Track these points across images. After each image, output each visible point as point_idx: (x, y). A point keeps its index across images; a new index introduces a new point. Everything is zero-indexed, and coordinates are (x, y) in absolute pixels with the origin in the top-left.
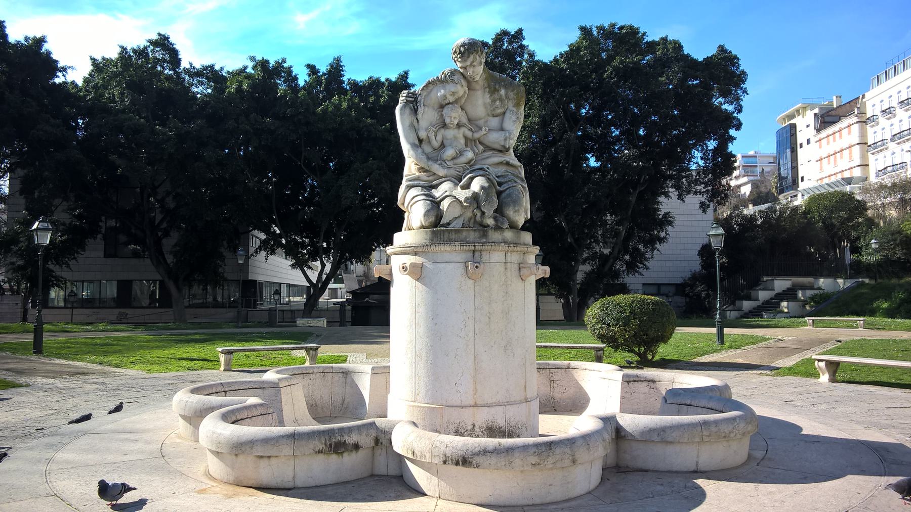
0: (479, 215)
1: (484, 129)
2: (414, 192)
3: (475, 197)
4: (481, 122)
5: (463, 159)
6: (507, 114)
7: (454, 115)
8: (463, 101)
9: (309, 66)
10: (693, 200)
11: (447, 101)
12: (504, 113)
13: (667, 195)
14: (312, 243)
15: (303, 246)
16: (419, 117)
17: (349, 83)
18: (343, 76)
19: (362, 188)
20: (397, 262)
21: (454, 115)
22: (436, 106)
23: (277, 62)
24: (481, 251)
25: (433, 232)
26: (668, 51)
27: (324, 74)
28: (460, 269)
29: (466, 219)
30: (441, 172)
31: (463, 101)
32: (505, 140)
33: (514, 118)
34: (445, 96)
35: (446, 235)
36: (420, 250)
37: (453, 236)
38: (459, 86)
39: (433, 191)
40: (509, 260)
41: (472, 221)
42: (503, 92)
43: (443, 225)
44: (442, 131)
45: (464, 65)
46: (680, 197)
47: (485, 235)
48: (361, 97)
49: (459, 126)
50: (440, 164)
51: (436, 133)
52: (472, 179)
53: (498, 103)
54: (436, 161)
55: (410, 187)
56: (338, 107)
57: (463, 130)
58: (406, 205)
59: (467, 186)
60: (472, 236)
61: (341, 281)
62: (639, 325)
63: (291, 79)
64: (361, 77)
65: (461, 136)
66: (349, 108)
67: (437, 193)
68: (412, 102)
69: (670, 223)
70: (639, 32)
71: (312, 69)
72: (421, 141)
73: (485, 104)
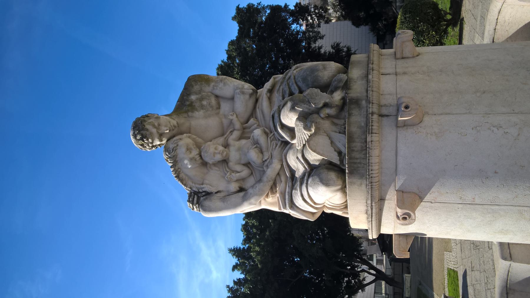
0: (327, 111)
1: (231, 117)
2: (299, 202)
3: (304, 118)
4: (225, 122)
5: (262, 140)
6: (217, 92)
7: (214, 151)
8: (200, 140)
9: (233, 270)
10: (324, 29)
11: (198, 157)
12: (217, 97)
13: (320, 48)
14: (347, 276)
15: (349, 282)
16: (214, 190)
17: (244, 244)
18: (240, 248)
19: (312, 240)
20: (391, 226)
21: (214, 151)
22: (205, 170)
23: (229, 291)
24: (380, 106)
25: (351, 173)
26: (233, 49)
27: (239, 260)
28: (405, 135)
29: (334, 128)
30: (276, 166)
31: (200, 140)
32: (243, 93)
33: (221, 85)
34: (191, 160)
35: (356, 155)
36: (376, 194)
37: (357, 145)
38: (181, 143)
39: (298, 174)
40: (391, 70)
41: (336, 121)
42: (193, 97)
43: (342, 161)
44: (231, 164)
45: (156, 135)
46: (322, 38)
47: (356, 102)
48: (253, 238)
49: (226, 146)
50: (267, 166)
51: (233, 171)
52: (283, 126)
53: (205, 103)
54: (264, 172)
55: (293, 205)
56: (258, 253)
57: (231, 141)
58: (314, 211)
59: (291, 131)
60: (357, 118)
61: (372, 256)
62: (424, 23)
63: (238, 282)
64: (241, 236)
65: (238, 143)
66: (259, 245)
67: (300, 169)
68: (199, 198)
69: (338, 45)
70: (221, 65)
71: (235, 268)
72: (241, 190)
73: (206, 117)
